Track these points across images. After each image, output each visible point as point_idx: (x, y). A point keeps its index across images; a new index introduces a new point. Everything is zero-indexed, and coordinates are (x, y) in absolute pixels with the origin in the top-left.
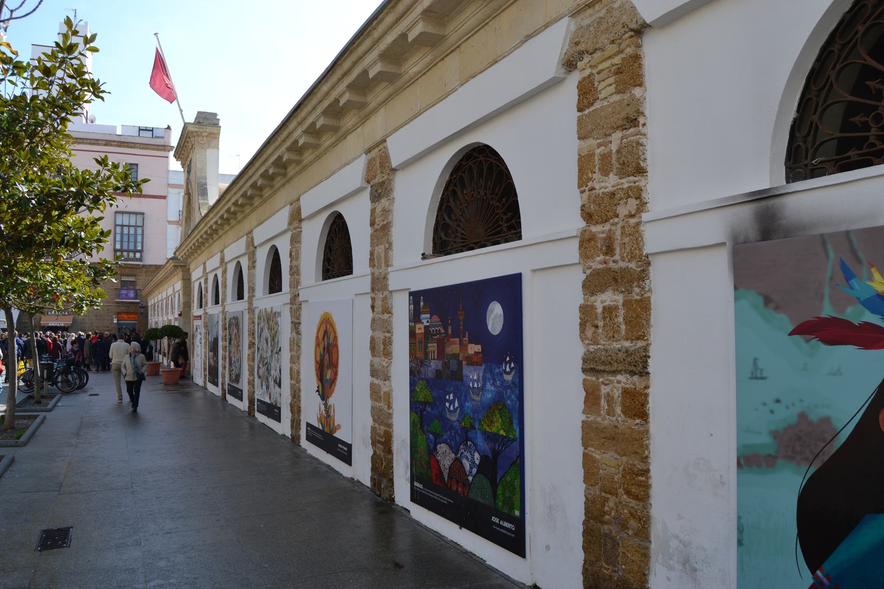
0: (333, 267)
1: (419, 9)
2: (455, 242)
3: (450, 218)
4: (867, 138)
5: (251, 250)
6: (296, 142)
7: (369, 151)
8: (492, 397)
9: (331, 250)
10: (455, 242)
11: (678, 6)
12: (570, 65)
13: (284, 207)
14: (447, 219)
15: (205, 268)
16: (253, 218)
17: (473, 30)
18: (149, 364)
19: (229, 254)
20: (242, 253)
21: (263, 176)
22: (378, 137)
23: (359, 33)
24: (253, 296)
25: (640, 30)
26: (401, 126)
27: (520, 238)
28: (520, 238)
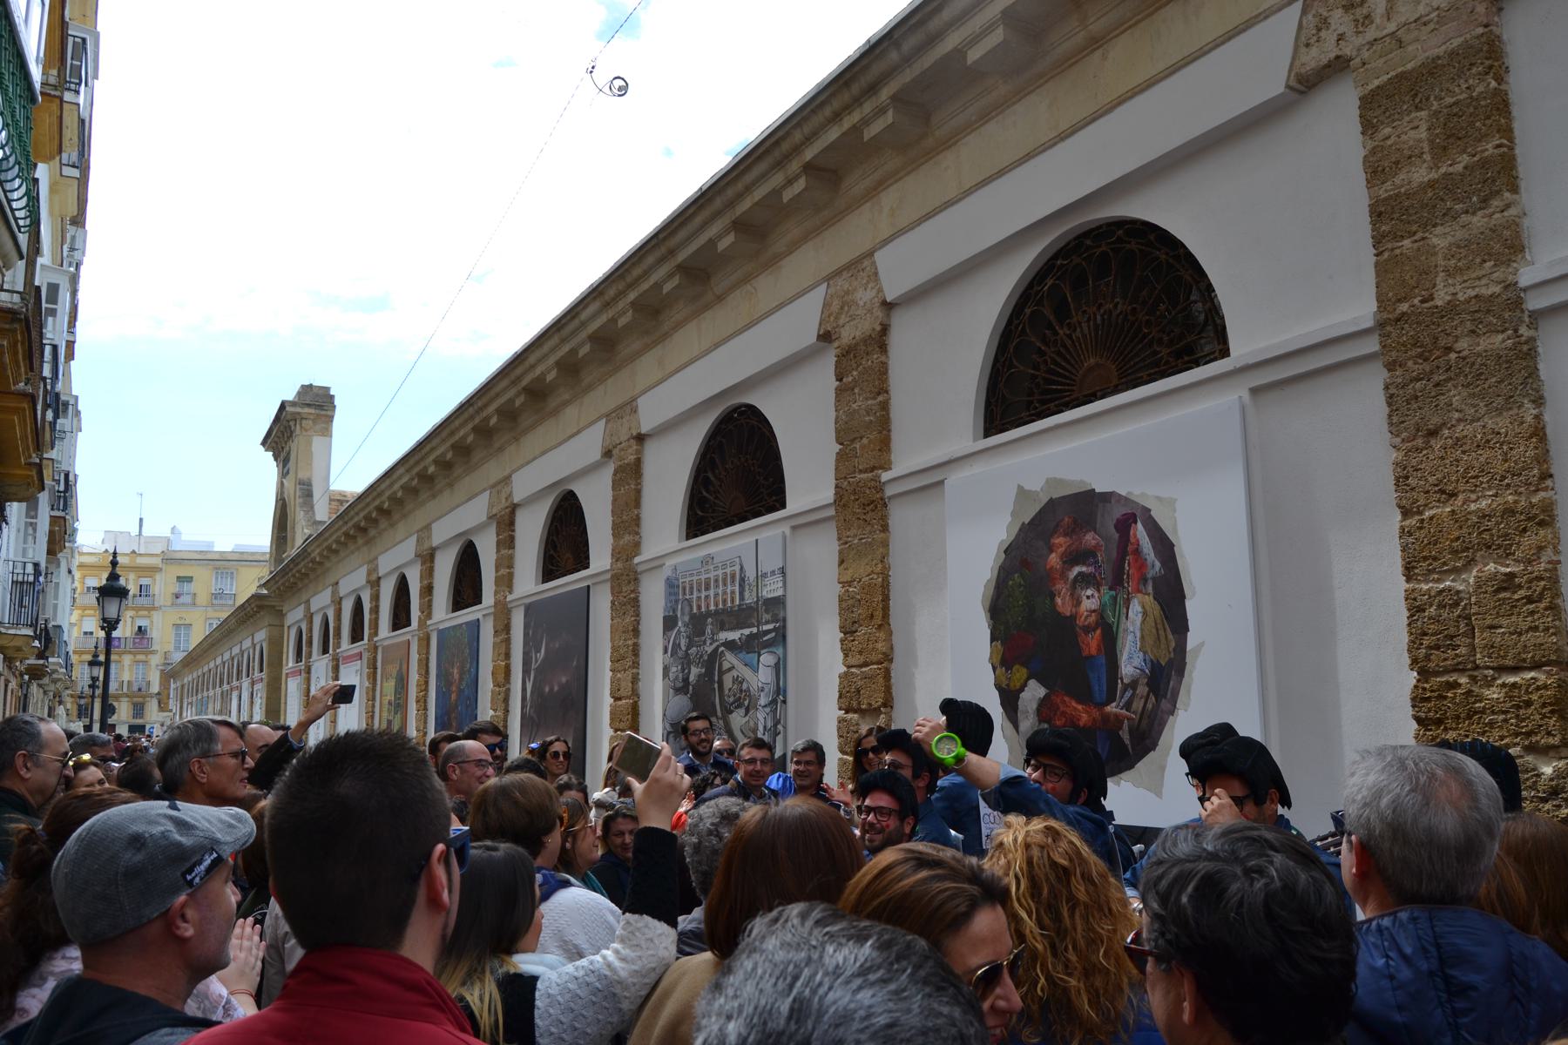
0: (557, 566)
1: (993, 11)
2: (712, 517)
3: (707, 492)
4: (1162, 358)
5: (310, 617)
6: (426, 468)
7: (828, 279)
8: (410, 740)
9: (555, 547)
10: (712, 517)
11: (958, 262)
12: (608, 454)
13: (360, 566)
14: (705, 493)
15: (308, 608)
16: (646, 367)
17: (1122, 24)
18: (827, 1012)
19: (186, 681)
20: (408, 559)
21: (365, 518)
22: (506, 473)
23: (455, 412)
24: (636, 547)
25: (641, 438)
26: (1001, 173)
27: (1225, 353)
28: (1225, 353)
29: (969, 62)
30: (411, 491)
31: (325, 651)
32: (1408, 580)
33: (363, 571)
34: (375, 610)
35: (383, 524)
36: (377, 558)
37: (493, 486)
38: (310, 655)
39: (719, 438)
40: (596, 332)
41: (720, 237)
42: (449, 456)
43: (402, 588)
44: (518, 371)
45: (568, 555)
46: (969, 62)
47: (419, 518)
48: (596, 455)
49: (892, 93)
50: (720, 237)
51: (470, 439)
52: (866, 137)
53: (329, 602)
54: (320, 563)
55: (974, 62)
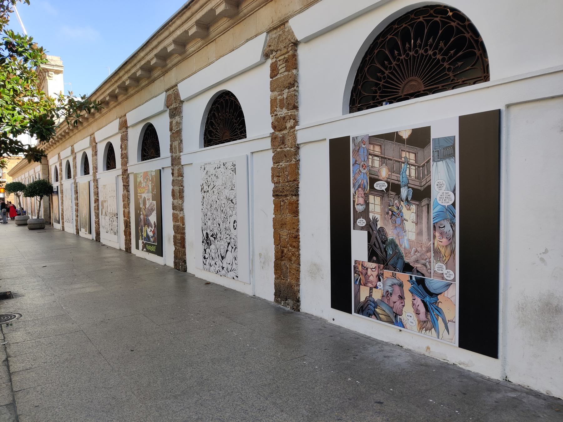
7: (167, 91)
12: (266, 55)
29: (137, 75)
30: (114, 96)
31: (69, 177)
32: (173, 210)
33: (88, 140)
34: (75, 167)
35: (67, 137)
36: (176, 85)
37: (90, 136)
38: (62, 178)
39: (217, 105)
40: (179, 37)
41: (152, 59)
42: (107, 98)
43: (110, 149)
44: (128, 67)
45: (152, 150)
46: (137, 75)
47: (90, 130)
48: (257, 56)
49: (140, 66)
50: (152, 59)
51: (117, 91)
52: (190, 34)
53: (88, 145)
54: (68, 133)
55: (192, 35)
